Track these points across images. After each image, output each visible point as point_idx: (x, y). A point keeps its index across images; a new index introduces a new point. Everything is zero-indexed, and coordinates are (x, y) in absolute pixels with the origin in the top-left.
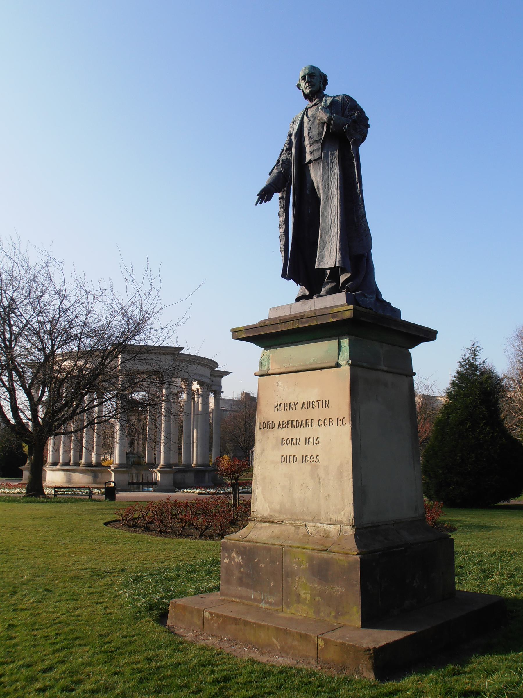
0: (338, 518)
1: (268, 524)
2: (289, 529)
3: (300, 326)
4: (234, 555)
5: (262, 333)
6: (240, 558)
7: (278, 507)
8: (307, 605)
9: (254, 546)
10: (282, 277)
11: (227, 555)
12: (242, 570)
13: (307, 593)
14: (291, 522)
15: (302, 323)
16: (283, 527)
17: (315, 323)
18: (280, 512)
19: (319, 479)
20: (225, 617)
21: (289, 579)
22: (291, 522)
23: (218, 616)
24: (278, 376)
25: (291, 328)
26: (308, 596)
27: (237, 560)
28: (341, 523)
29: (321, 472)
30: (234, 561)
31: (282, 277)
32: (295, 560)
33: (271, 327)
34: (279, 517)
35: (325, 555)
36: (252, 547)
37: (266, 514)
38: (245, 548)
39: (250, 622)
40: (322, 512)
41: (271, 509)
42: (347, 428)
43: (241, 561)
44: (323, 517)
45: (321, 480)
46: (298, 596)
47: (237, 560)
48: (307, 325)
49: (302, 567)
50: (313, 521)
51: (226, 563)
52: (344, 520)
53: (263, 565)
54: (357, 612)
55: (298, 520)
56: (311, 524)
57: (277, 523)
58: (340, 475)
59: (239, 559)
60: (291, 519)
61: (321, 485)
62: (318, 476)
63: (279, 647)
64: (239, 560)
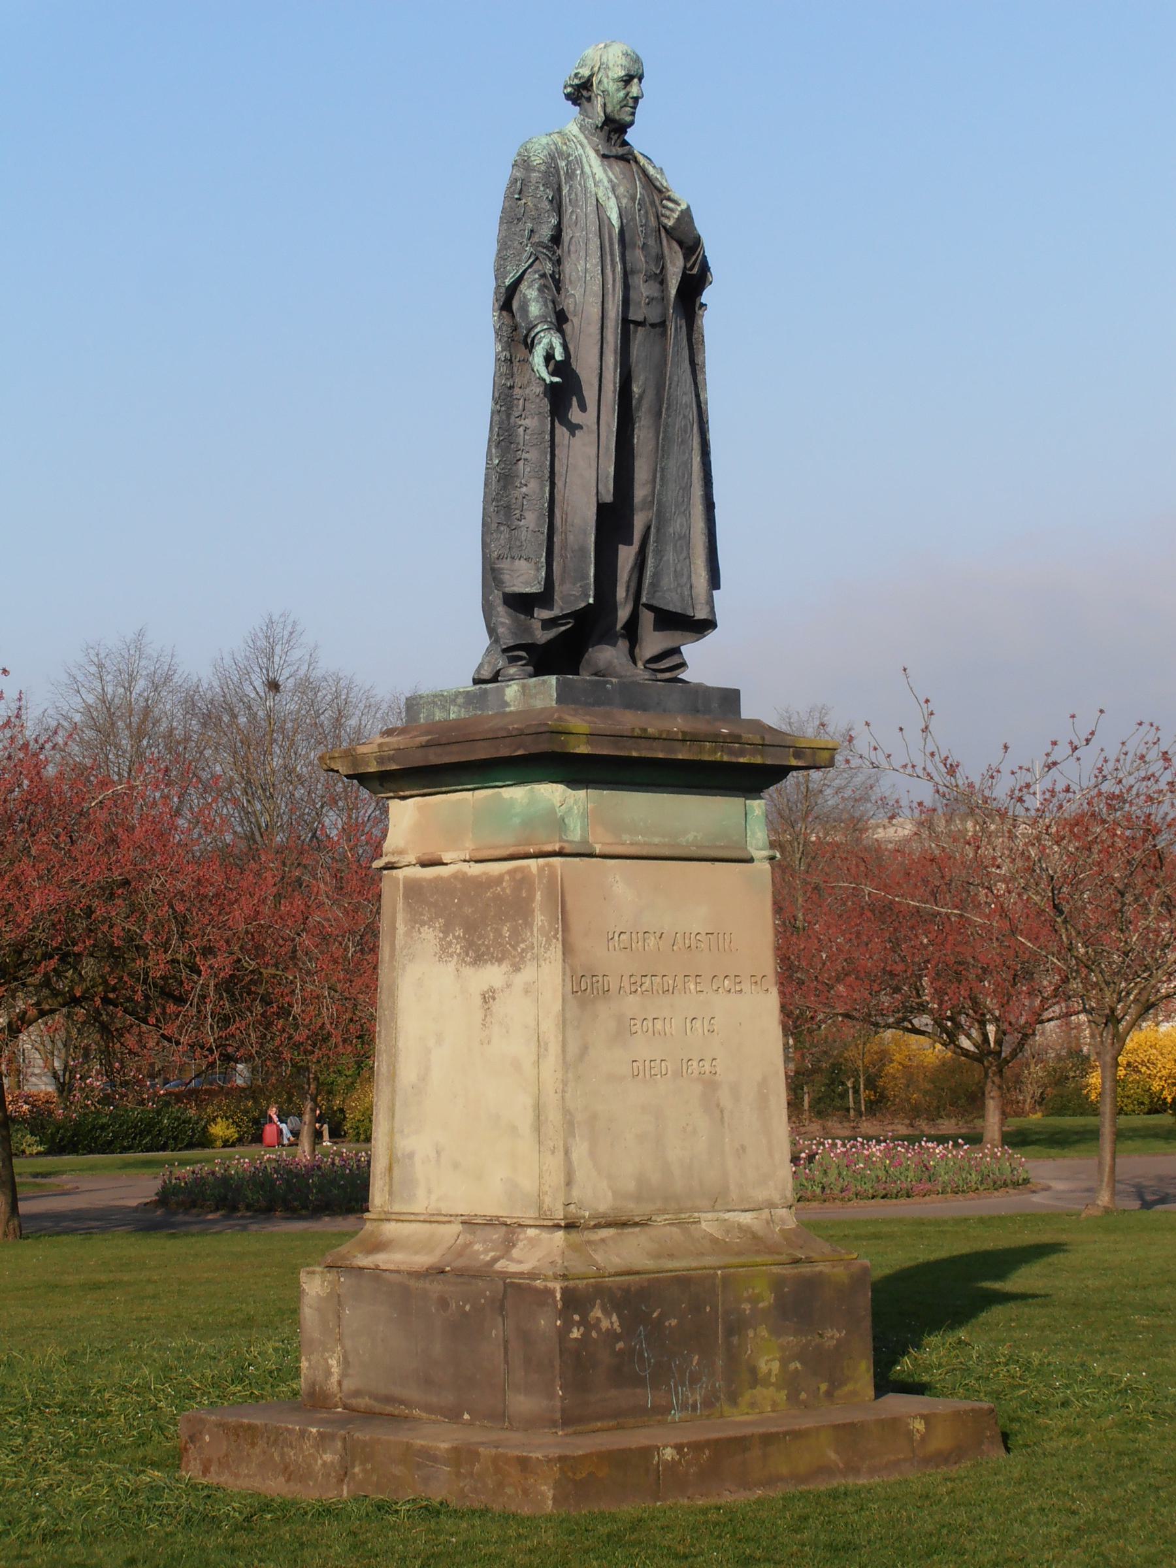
0: (761, 1195)
1: (611, 1231)
2: (664, 1231)
3: (726, 758)
4: (597, 1313)
5: (634, 754)
6: (615, 1318)
7: (631, 1186)
8: (772, 1384)
9: (649, 1280)
11: (577, 1317)
12: (620, 1345)
13: (771, 1360)
14: (667, 1216)
15: (731, 752)
18: (638, 1198)
19: (722, 1112)
20: (717, 1441)
21: (735, 1340)
22: (667, 1216)
23: (697, 1447)
26: (776, 1366)
27: (605, 1324)
28: (772, 1205)
30: (599, 1330)
32: (745, 1295)
34: (636, 1210)
35: (806, 1270)
36: (646, 1284)
37: (603, 1207)
38: (626, 1290)
39: (777, 1434)
40: (732, 1187)
41: (614, 1193)
42: (770, 1001)
43: (616, 1325)
44: (734, 1195)
45: (726, 1114)
46: (753, 1371)
47: (605, 1324)
49: (761, 1305)
51: (576, 1339)
52: (776, 1198)
53: (674, 1322)
54: (868, 1371)
55: (681, 1211)
56: (710, 1216)
57: (636, 1224)
58: (763, 1099)
59: (610, 1322)
60: (664, 1211)
61: (726, 1125)
62: (718, 1105)
63: (841, 1465)
64: (612, 1323)
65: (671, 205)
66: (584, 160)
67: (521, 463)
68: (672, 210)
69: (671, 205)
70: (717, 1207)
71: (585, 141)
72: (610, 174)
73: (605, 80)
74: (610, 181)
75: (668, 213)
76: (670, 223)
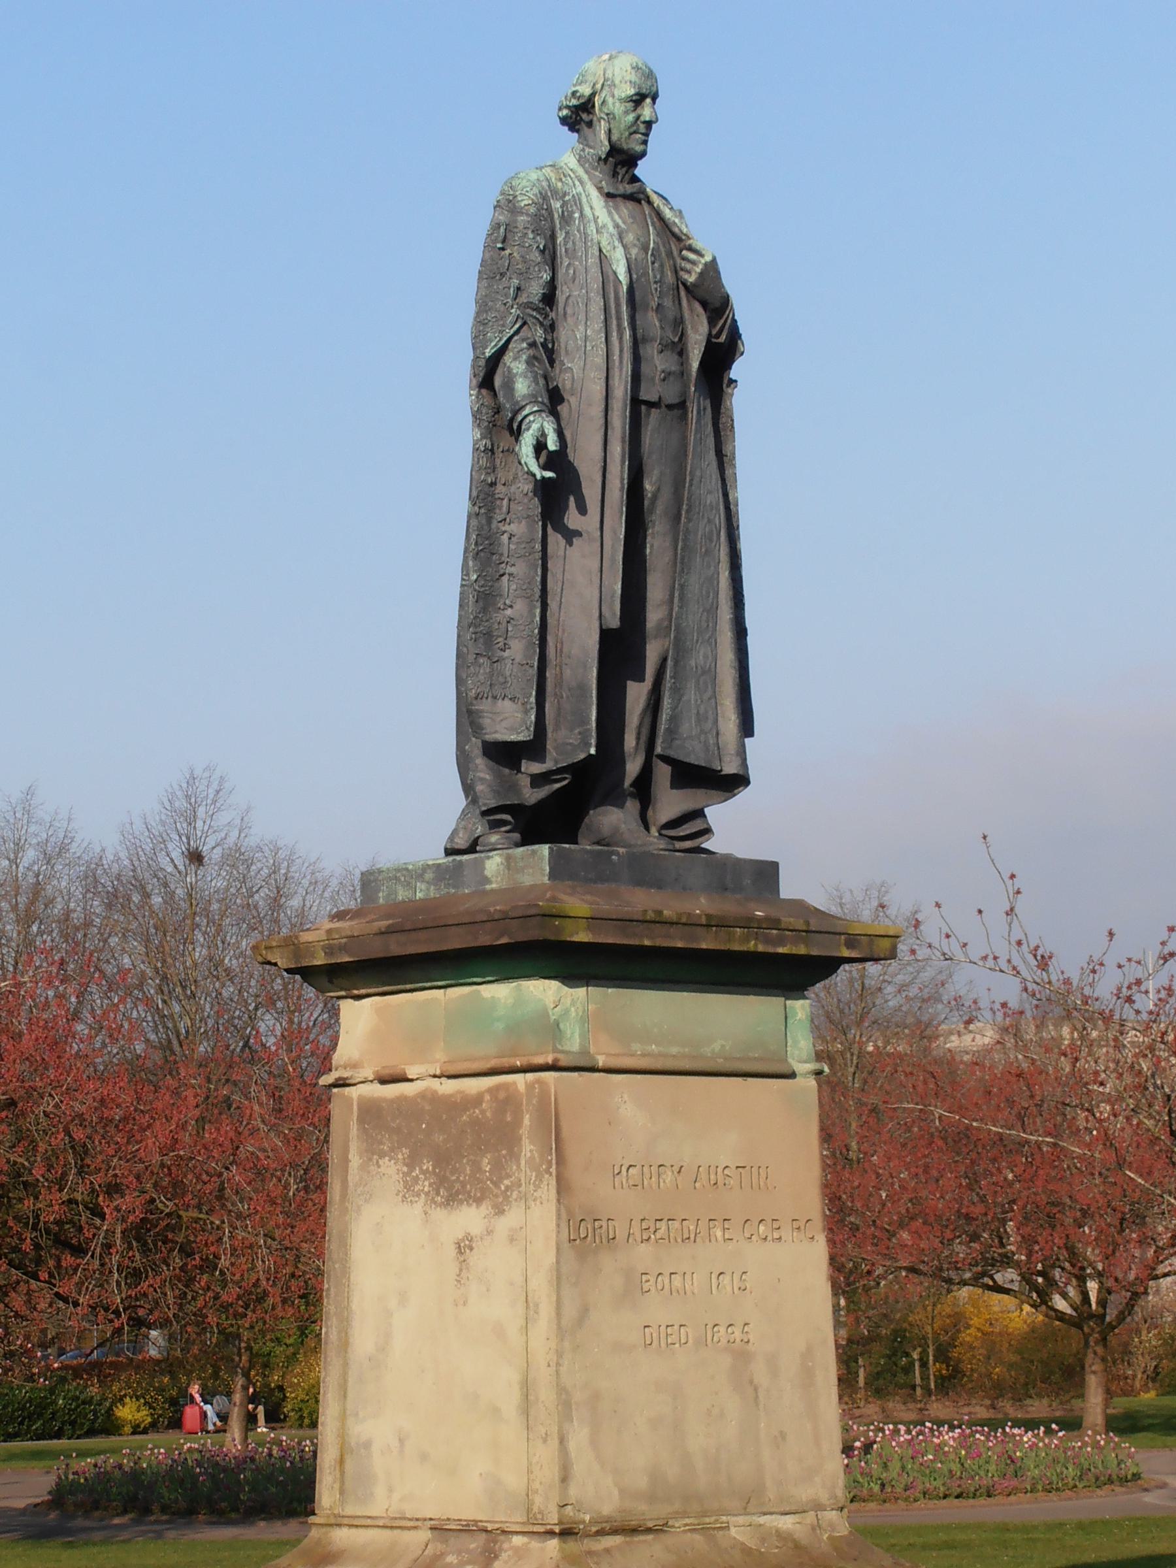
1: (617, 1540)
3: (761, 948)
5: (647, 943)
7: (642, 1482)
10: (775, 866)
14: (687, 1521)
15: (768, 940)
16: (667, 1540)
17: (802, 950)
19: (756, 1389)
22: (687, 1521)
24: (639, 1076)
25: (736, 947)
28: (818, 1507)
29: (759, 1372)
31: (775, 866)
33: (422, 935)
34: (648, 1513)
41: (622, 1491)
48: (780, 950)
50: (745, 1512)
52: (824, 1497)
55: (705, 1514)
56: (741, 1520)
57: (649, 1530)
58: (807, 1374)
60: (685, 1514)
61: (761, 1406)
62: (751, 1382)
65: (692, 256)
66: (584, 200)
67: (505, 578)
68: (694, 263)
69: (692, 256)
70: (751, 1509)
71: (585, 177)
72: (616, 217)
73: (610, 100)
74: (617, 226)
75: (688, 266)
76: (691, 279)
